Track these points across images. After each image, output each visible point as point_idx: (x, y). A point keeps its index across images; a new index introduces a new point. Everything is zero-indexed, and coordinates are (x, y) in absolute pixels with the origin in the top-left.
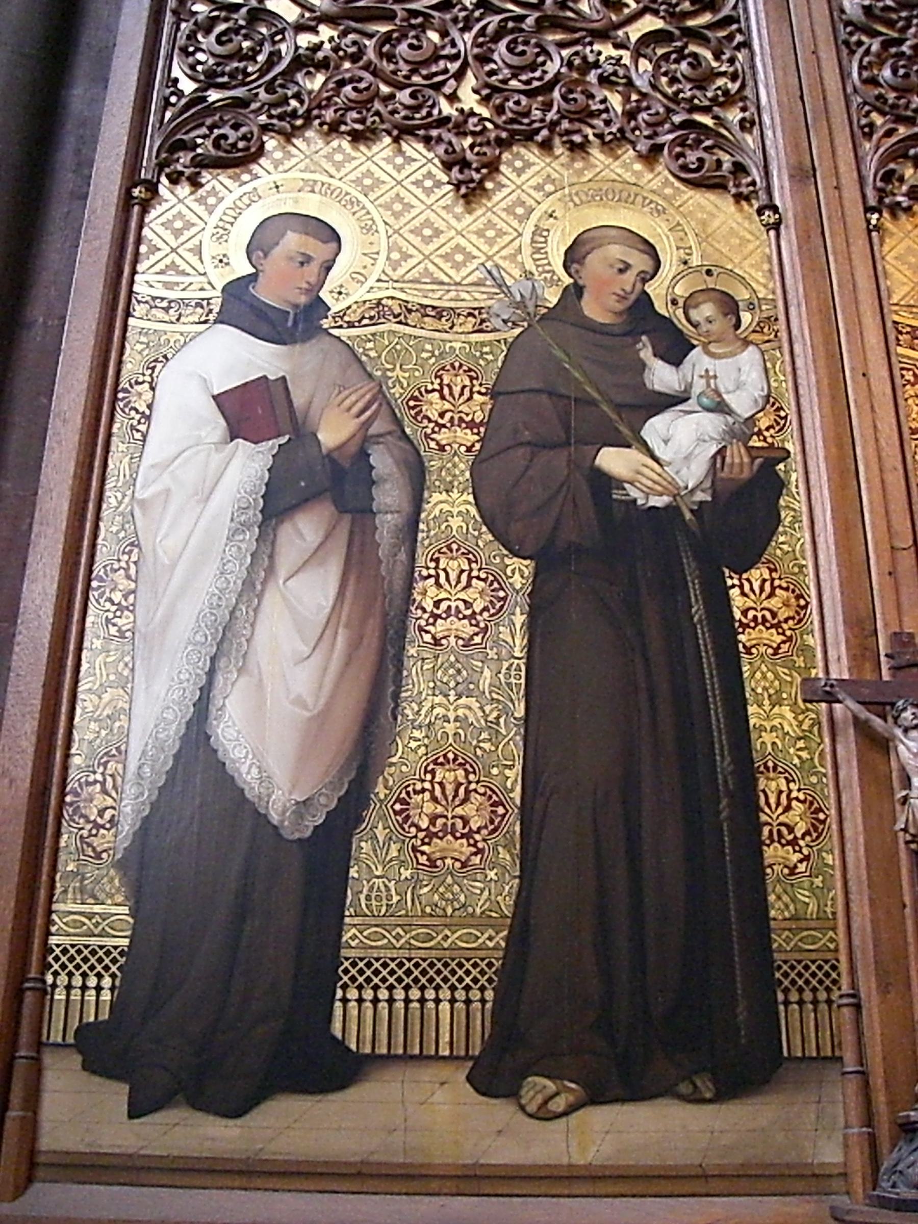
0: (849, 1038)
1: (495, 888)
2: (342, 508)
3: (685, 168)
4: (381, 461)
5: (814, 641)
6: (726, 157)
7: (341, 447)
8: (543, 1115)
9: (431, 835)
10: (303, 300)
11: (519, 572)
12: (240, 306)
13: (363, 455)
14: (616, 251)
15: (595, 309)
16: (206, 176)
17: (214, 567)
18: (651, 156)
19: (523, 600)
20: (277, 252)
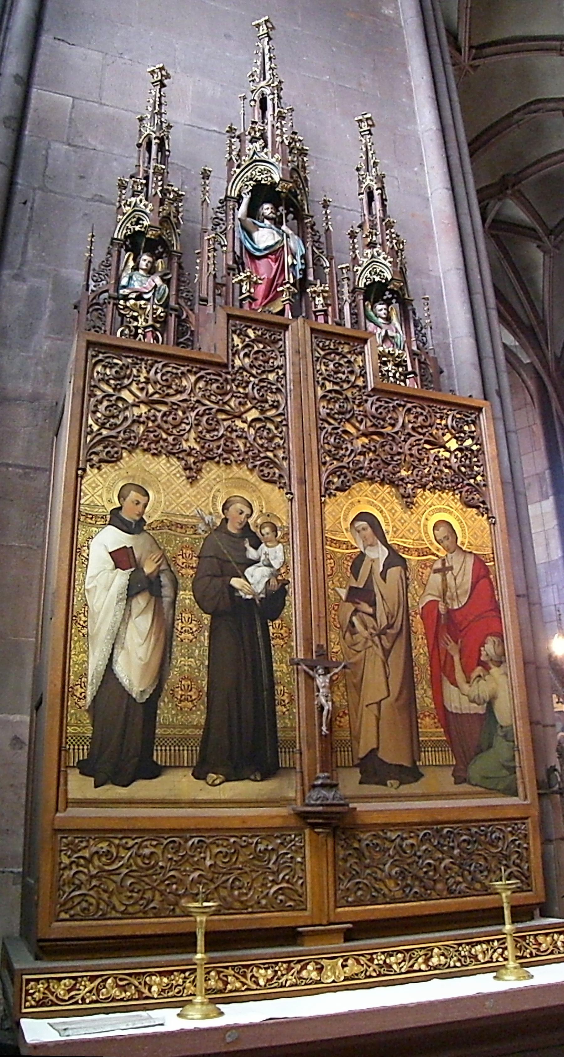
0: (298, 762)
1: (199, 717)
2: (152, 594)
3: (263, 476)
4: (164, 579)
5: (293, 644)
6: (277, 471)
7: (151, 573)
8: (213, 785)
9: (181, 701)
10: (137, 518)
11: (206, 619)
12: (116, 519)
13: (159, 577)
14: (239, 506)
15: (232, 528)
16: (103, 465)
17: (111, 614)
18: (251, 470)
19: (208, 628)
20: (128, 499)
